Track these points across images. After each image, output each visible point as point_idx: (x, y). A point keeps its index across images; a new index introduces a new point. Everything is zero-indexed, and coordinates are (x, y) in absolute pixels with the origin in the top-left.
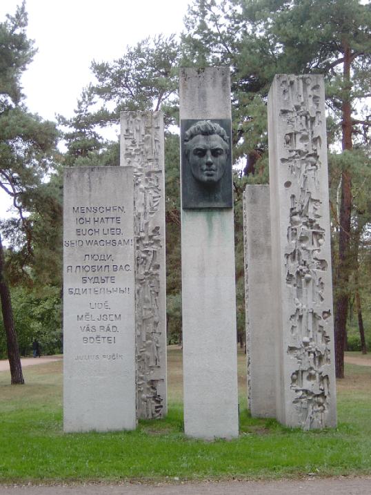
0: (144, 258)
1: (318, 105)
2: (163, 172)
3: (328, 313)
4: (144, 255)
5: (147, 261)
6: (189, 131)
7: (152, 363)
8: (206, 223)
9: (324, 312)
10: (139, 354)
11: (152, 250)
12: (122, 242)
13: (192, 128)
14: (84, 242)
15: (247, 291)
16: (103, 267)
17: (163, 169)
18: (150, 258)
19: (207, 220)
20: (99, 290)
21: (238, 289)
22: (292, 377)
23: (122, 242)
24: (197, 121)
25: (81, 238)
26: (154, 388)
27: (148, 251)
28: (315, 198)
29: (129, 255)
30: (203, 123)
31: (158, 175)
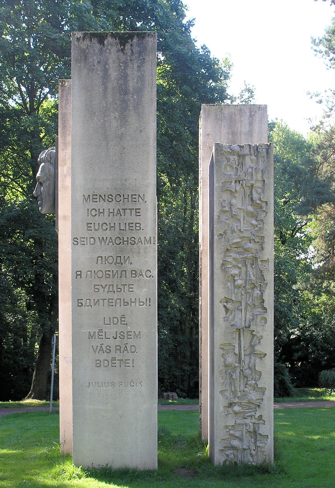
20: (114, 301)
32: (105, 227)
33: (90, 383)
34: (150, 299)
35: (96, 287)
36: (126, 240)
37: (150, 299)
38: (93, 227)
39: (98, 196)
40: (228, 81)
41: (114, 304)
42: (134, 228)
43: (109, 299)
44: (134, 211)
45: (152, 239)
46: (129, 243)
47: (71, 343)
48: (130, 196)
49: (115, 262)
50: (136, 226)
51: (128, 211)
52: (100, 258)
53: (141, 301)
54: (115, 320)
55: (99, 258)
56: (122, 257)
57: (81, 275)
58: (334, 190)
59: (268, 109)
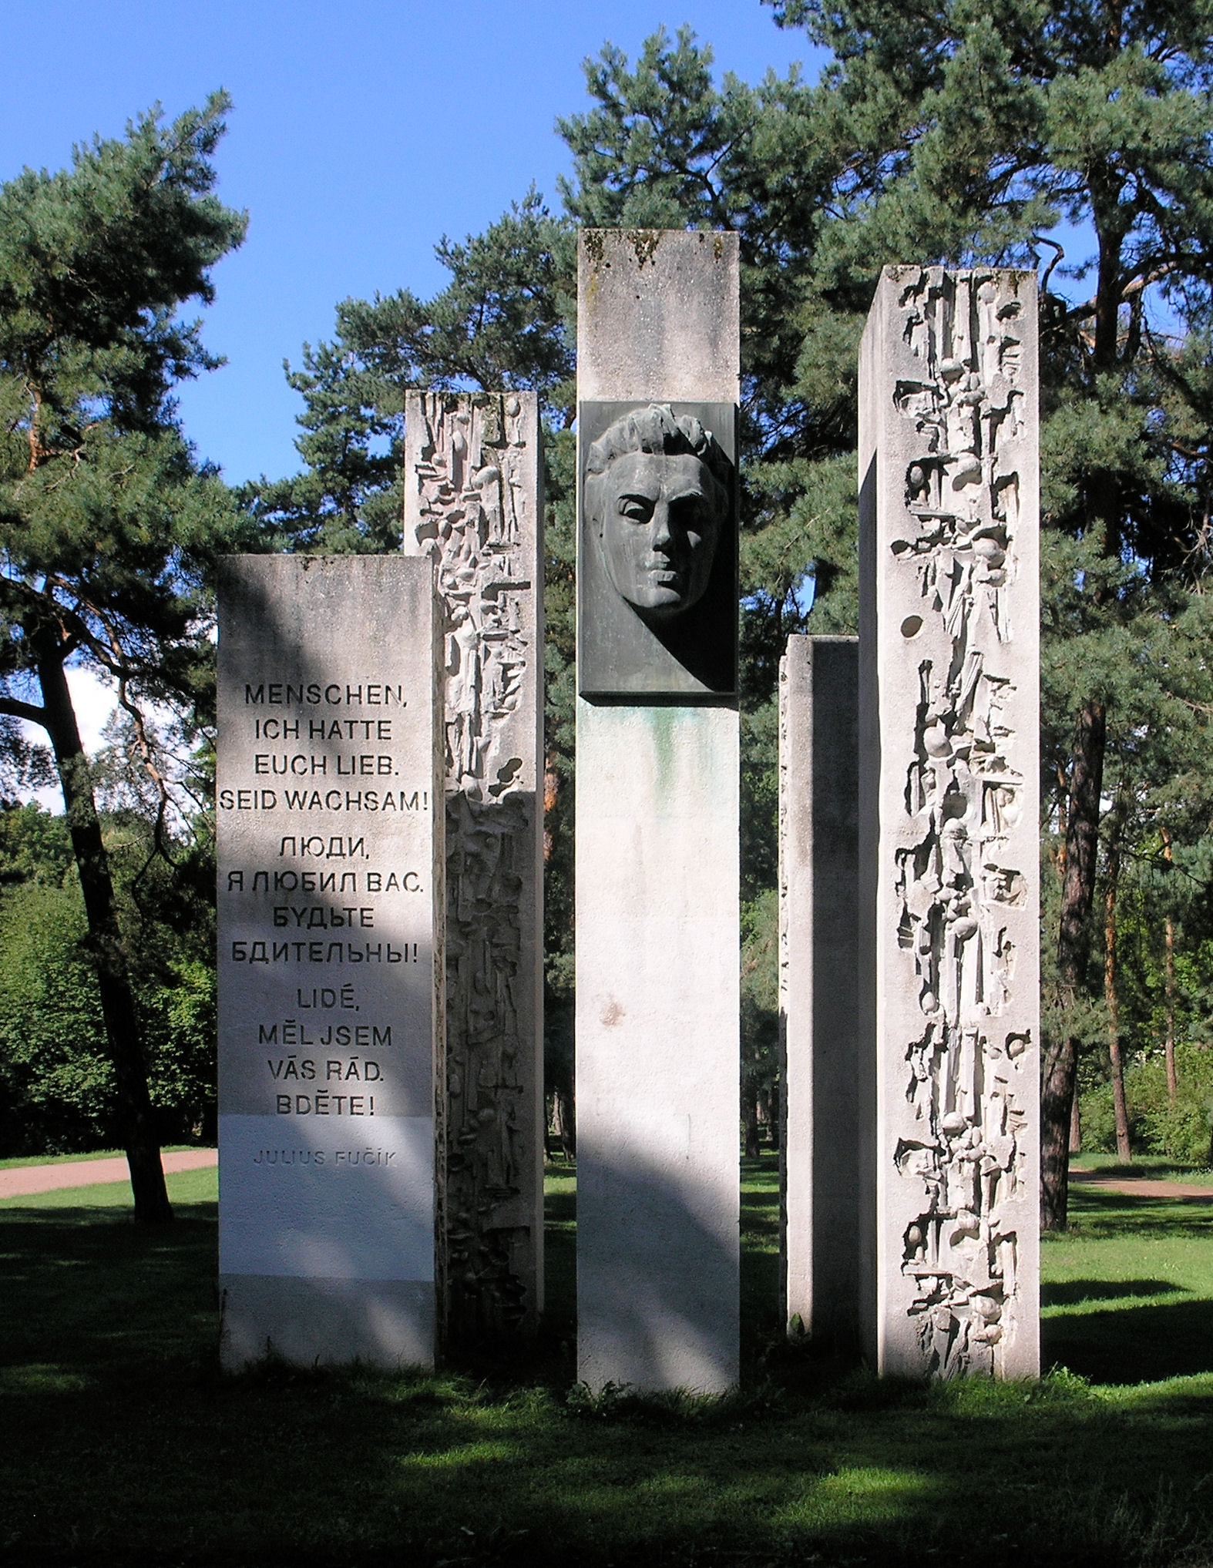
0: (476, 856)
1: (952, 1317)
2: (534, 585)
3: (1025, 1038)
4: (472, 847)
5: (483, 868)
6: (602, 440)
7: (496, 1179)
8: (650, 742)
9: (1011, 1038)
10: (456, 1150)
11: (498, 831)
12: (396, 798)
13: (611, 432)
14: (280, 796)
15: (784, 965)
16: (338, 879)
17: (533, 577)
18: (491, 858)
19: (656, 729)
20: (325, 948)
21: (748, 971)
22: (906, 1236)
23: (396, 798)
24: (629, 406)
25: (271, 781)
26: (502, 1255)
27: (487, 835)
28: (1051, 247)
29: (418, 841)
30: (649, 413)
31: (517, 595)
32: (300, 765)
33: (280, 1152)
34: (299, 991)
35: (279, 913)
36: (357, 799)
37: (299, 991)
38: (271, 765)
39: (284, 689)
40: (716, 72)
41: (324, 955)
42: (375, 769)
43: (312, 944)
44: (373, 727)
45: (421, 796)
46: (362, 806)
47: (809, 714)
48: (365, 692)
49: (327, 851)
50: (380, 765)
51: (360, 728)
52: (291, 841)
53: (353, 950)
54: (328, 996)
55: (287, 841)
56: (346, 841)
57: (241, 882)
58: (1210, 466)
59: (225, 1234)
